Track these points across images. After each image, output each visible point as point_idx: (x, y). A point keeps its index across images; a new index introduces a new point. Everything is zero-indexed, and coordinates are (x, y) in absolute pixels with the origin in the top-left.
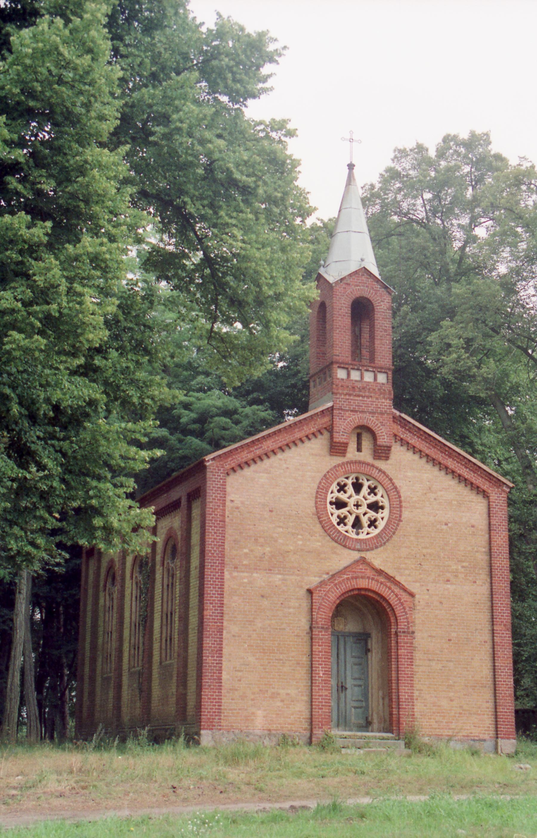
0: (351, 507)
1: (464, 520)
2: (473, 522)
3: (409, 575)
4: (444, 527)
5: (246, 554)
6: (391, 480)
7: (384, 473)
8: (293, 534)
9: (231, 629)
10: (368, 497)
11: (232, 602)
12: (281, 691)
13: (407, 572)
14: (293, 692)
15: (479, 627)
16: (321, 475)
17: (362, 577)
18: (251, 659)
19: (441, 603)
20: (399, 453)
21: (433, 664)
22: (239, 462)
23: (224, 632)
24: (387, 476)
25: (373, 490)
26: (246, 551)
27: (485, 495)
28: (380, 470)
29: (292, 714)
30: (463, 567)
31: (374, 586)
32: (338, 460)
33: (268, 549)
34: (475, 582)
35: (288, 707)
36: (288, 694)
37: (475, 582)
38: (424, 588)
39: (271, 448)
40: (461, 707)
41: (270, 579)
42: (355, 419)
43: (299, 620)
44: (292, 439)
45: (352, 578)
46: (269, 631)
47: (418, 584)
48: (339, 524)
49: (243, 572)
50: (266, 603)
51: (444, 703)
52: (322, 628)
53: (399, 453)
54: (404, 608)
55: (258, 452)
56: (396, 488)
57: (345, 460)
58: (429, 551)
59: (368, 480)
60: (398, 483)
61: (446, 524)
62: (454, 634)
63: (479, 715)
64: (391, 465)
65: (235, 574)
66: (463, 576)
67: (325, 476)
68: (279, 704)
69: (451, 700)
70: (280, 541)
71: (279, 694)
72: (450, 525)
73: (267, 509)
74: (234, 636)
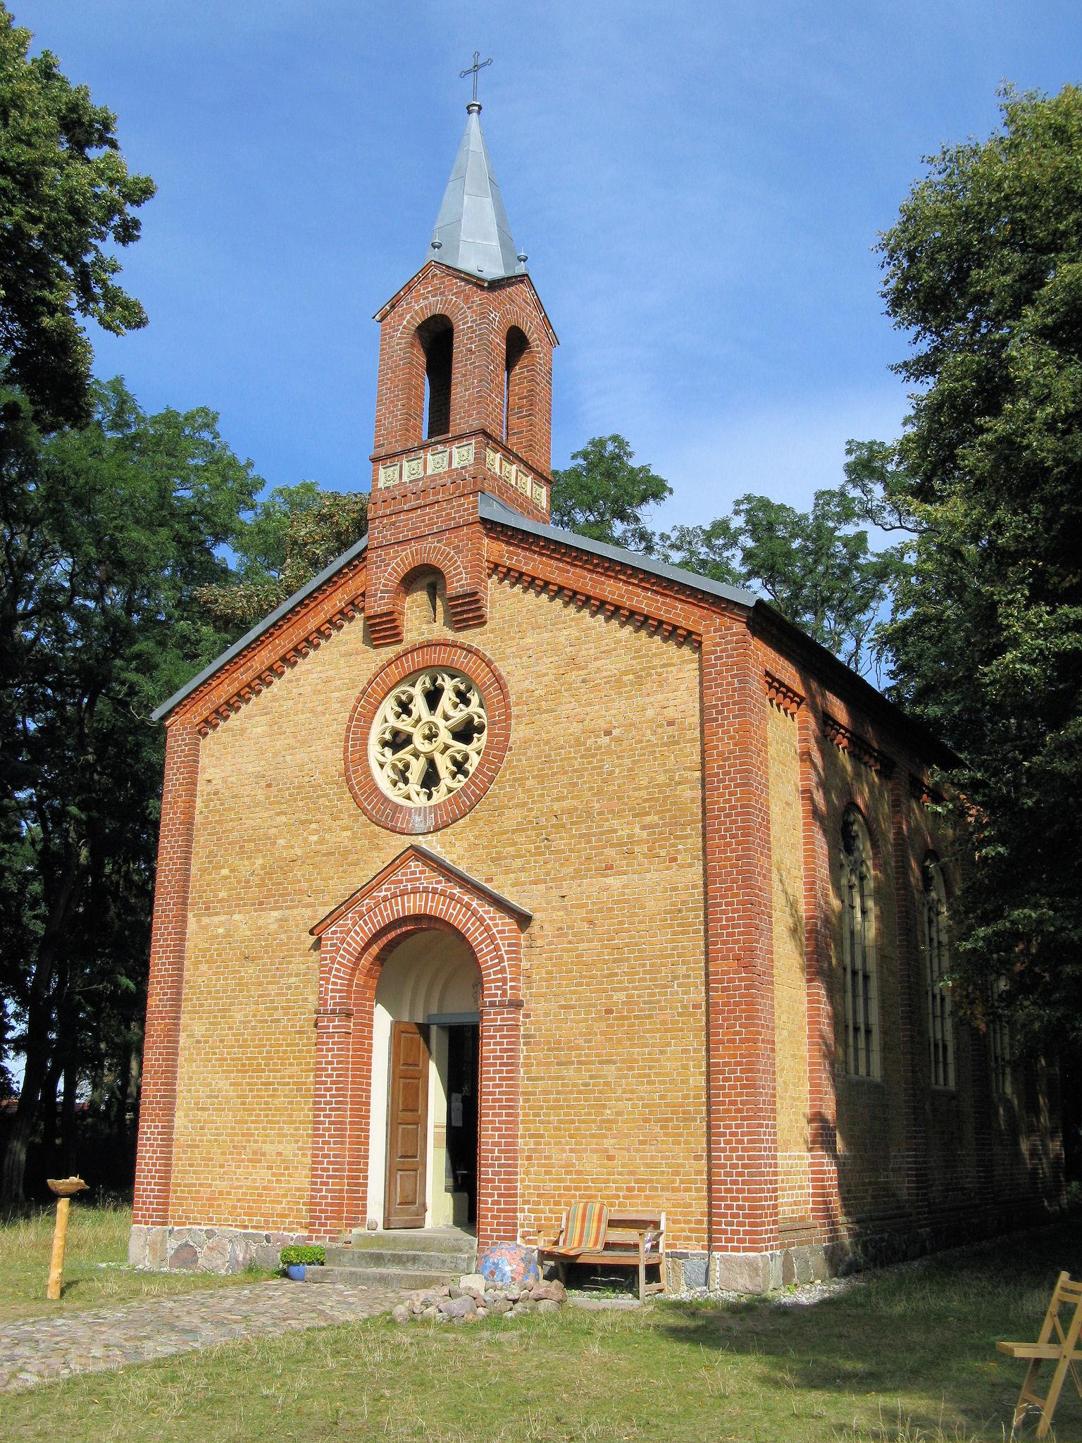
0: (419, 743)
1: (650, 713)
2: (670, 713)
3: (522, 870)
4: (605, 740)
5: (226, 878)
6: (489, 664)
7: (476, 653)
8: (302, 823)
9: (193, 1027)
10: (415, 716)
11: (197, 975)
12: (268, 1148)
13: (518, 863)
14: (289, 1149)
15: (682, 970)
16: (356, 693)
17: (415, 891)
18: (224, 1085)
19: (591, 922)
20: (503, 601)
21: (570, 1072)
22: (213, 707)
23: (183, 1035)
24: (483, 658)
25: (463, 698)
26: (225, 872)
27: (688, 638)
28: (469, 650)
29: (285, 1196)
30: (644, 828)
31: (435, 907)
32: (389, 652)
33: (260, 861)
34: (674, 860)
35: (278, 1181)
36: (279, 1154)
37: (674, 860)
38: (556, 893)
39: (267, 663)
40: (632, 1173)
41: (260, 922)
42: (404, 560)
43: (306, 1000)
44: (303, 634)
45: (395, 896)
46: (254, 1028)
47: (542, 887)
48: (466, 774)
49: (217, 914)
50: (251, 970)
51: (591, 1163)
52: (333, 1012)
53: (503, 601)
54: (497, 949)
55: (246, 678)
56: (498, 679)
57: (399, 648)
58: (565, 804)
59: (413, 685)
60: (502, 668)
61: (608, 733)
62: (620, 997)
63: (674, 1190)
64: (492, 631)
65: (205, 920)
66: (645, 848)
67: (364, 692)
68: (267, 1175)
69: (611, 1158)
70: (281, 842)
71: (264, 1154)
72: (615, 732)
73: (263, 784)
74: (198, 1042)
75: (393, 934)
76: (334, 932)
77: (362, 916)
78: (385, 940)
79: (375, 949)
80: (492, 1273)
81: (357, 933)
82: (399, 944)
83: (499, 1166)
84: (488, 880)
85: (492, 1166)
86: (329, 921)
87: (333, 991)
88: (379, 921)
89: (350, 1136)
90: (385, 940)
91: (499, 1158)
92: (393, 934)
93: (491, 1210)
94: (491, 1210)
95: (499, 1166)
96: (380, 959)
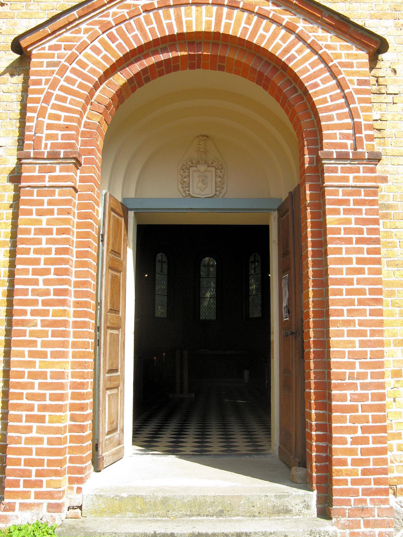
52: (53, 156)
75: (153, 60)
76: (57, 47)
77: (106, 28)
78: (137, 67)
79: (120, 79)
80: (351, 473)
81: (97, 51)
82: (176, 69)
83: (364, 386)
84: (308, 507)
85: (353, 386)
86: (48, 29)
87: (50, 127)
88: (136, 38)
89: (75, 345)
90: (137, 67)
91: (362, 376)
92: (153, 60)
93: (352, 452)
94: (352, 452)
95: (364, 386)
96: (121, 95)
